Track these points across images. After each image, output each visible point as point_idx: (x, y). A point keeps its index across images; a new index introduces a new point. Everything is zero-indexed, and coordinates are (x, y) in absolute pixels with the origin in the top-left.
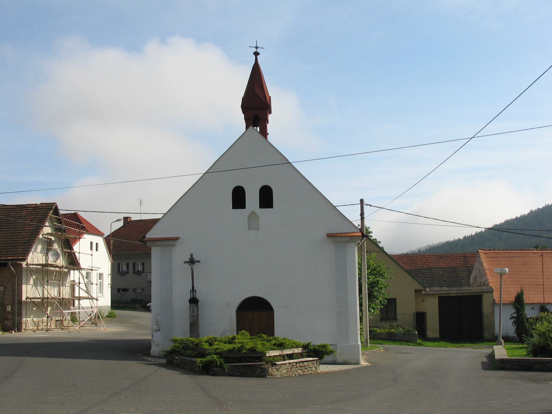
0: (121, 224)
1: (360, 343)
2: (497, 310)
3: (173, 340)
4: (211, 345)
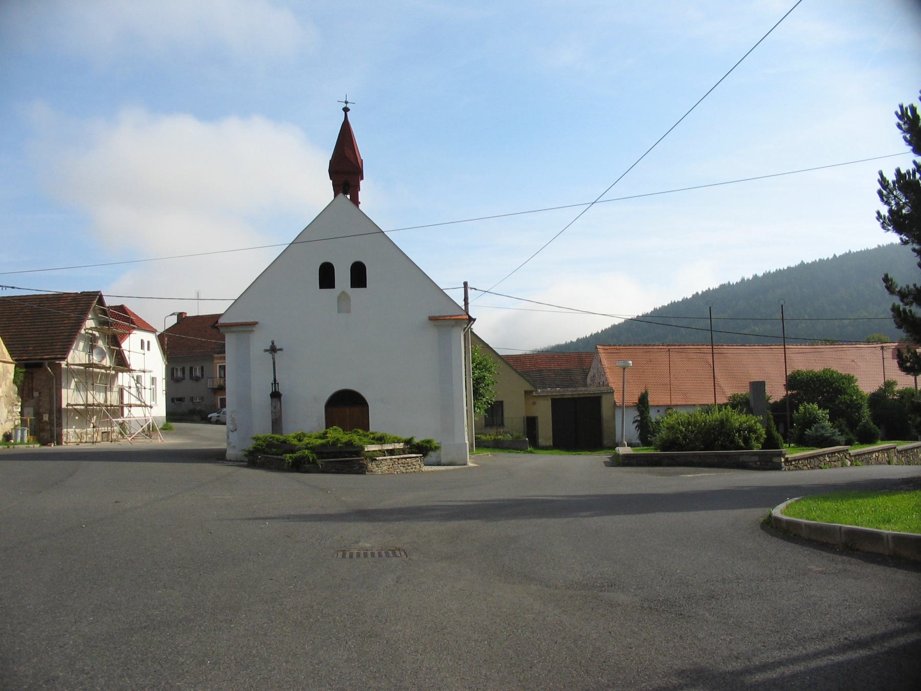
0: (174, 320)
1: (467, 442)
2: (618, 413)
3: (254, 438)
4: (300, 440)
